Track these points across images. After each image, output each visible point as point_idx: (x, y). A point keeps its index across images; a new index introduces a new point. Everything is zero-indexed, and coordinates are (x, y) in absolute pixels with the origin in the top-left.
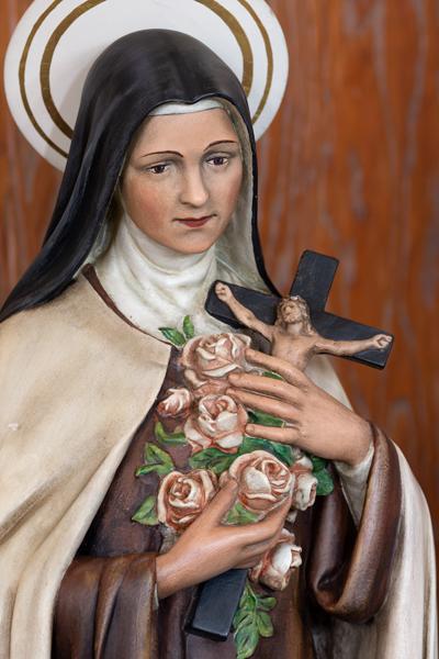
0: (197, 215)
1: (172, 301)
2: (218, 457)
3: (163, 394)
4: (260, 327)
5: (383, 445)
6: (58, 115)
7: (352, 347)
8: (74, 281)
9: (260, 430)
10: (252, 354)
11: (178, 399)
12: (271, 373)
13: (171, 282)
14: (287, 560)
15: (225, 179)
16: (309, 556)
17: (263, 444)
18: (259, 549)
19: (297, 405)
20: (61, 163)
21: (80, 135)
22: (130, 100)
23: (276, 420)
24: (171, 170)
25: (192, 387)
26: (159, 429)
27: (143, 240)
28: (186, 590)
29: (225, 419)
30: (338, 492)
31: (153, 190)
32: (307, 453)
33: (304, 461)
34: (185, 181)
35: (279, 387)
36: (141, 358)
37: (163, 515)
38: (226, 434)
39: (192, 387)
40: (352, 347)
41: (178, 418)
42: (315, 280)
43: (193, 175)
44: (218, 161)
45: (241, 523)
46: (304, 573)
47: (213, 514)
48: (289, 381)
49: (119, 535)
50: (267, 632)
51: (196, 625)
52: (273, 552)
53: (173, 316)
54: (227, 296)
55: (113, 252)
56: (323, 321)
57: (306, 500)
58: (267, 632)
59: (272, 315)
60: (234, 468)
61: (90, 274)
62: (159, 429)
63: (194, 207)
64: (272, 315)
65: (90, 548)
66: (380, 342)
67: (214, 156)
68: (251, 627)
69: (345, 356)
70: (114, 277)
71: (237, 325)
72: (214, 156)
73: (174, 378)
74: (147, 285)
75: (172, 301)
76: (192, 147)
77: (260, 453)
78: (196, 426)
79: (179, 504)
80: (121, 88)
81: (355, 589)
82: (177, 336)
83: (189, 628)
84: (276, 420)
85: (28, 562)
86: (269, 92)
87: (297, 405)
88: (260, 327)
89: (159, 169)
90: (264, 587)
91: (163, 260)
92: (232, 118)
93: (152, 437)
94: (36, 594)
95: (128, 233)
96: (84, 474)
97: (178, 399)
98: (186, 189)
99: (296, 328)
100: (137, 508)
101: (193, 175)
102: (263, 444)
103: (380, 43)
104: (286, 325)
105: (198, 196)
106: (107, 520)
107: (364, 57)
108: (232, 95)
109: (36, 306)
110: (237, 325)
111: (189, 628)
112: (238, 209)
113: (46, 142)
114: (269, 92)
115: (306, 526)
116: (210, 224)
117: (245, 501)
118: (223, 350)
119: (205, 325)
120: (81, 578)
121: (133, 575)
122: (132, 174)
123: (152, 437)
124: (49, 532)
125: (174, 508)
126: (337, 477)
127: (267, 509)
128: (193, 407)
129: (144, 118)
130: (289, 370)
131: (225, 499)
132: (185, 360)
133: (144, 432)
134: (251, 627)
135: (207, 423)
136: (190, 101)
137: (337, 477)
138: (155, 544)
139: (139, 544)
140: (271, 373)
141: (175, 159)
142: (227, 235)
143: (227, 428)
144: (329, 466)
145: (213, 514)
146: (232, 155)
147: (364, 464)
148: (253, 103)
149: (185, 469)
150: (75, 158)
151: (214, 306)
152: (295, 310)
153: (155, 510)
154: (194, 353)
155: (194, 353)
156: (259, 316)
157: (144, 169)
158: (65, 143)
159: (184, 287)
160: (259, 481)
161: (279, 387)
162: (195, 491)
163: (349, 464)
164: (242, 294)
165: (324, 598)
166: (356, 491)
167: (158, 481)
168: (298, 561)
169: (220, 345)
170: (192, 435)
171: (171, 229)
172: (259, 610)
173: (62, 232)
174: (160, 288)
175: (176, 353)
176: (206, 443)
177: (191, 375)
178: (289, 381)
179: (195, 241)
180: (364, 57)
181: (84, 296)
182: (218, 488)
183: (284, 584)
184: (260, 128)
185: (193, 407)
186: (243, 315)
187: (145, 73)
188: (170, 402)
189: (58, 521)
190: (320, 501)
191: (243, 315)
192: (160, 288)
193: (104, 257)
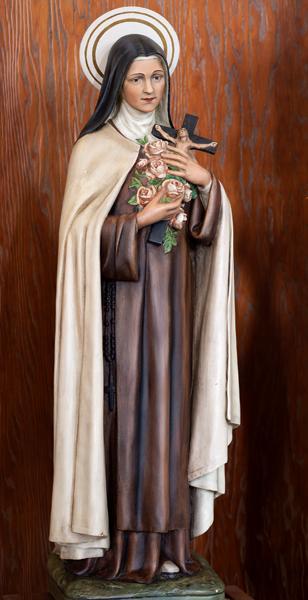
0: (149, 97)
1: (140, 130)
2: (158, 181)
3: (138, 161)
4: (172, 139)
5: (215, 180)
6: (113, 338)
7: (204, 146)
8: (105, 125)
9: (172, 172)
10: (169, 147)
11: (143, 162)
12: (175, 153)
13: (139, 123)
14: (182, 218)
15: (159, 85)
16: (189, 217)
17: (174, 177)
18: (172, 212)
19: (185, 164)
20: (99, 87)
21: (106, 76)
22: (126, 56)
23: (178, 169)
24: (140, 81)
25: (148, 159)
26: (136, 172)
27: (129, 108)
28: (146, 226)
29: (160, 168)
30: (199, 197)
31: (134, 88)
32: (189, 182)
33: (187, 184)
34: (145, 85)
35: (178, 157)
36: (129, 148)
37: (138, 201)
38: (160, 173)
39: (148, 159)
40: (204, 146)
41: (143, 169)
42: (190, 123)
43: (148, 81)
44: (157, 78)
45: (166, 202)
46: (188, 223)
47: (157, 199)
48: (181, 155)
49: (122, 208)
50: (175, 244)
51: (151, 240)
52: (178, 215)
53: (141, 136)
54: (159, 129)
55: (119, 115)
56: (192, 137)
57: (188, 198)
58: (175, 244)
59: (175, 134)
60: (163, 184)
61: (111, 122)
62: (136, 172)
63: (149, 94)
64: (175, 134)
65: (113, 212)
66: (213, 144)
67: (155, 76)
68: (169, 242)
69: (201, 150)
70: (119, 122)
71: (164, 139)
72: (155, 76)
73: (141, 155)
74: (131, 125)
75: (140, 130)
76: (148, 72)
77: (172, 180)
78: (149, 170)
79: (144, 197)
80: (122, 53)
81: (205, 230)
82: (142, 142)
83: (148, 241)
84: (178, 169)
85: (91, 217)
86: (174, 56)
87: (185, 164)
88: (172, 139)
89: (136, 80)
90: (174, 229)
91: (137, 116)
92: (162, 64)
93: (134, 175)
94: (95, 227)
95: (125, 107)
96: (110, 188)
97: (143, 162)
98: (145, 87)
99: (184, 139)
100: (129, 199)
101: (148, 81)
102: (174, 177)
103: (204, 73)
104: (180, 138)
105: (150, 90)
106: (119, 203)
107: (198, 78)
108: (162, 56)
109: (92, 132)
110: (164, 139)
111: (148, 241)
112: (163, 99)
113: (95, 81)
114: (174, 56)
115: (188, 207)
116: (154, 101)
117: (168, 196)
118: (159, 146)
119: (151, 138)
120: (110, 222)
121: (129, 220)
122: (126, 83)
123: (134, 175)
124: (98, 207)
125: (143, 199)
126: (199, 192)
127: (175, 198)
128: (149, 165)
129: (131, 62)
130: (182, 152)
131: (160, 194)
132: (145, 150)
133: (131, 173)
134: (169, 242)
135: (154, 170)
136: (147, 56)
137: (199, 192)
138: (136, 210)
139: (130, 210)
140: (175, 153)
141: (142, 77)
142: (158, 108)
143: (160, 171)
144: (196, 187)
145: (157, 199)
146: (162, 76)
147: (209, 186)
148: (169, 60)
149: (146, 186)
150: (104, 86)
151: (155, 132)
152: (184, 133)
153: (136, 200)
154: (149, 147)
155: (149, 147)
156: (171, 135)
157: (131, 80)
158: (101, 80)
159: (144, 125)
160: (172, 188)
161: (178, 157)
162: (150, 192)
163: (202, 186)
164: (164, 129)
165: (194, 234)
166: (205, 197)
167: (137, 190)
168: (186, 219)
169: (158, 144)
170: (148, 174)
171: (140, 104)
172: (238, 30)
173: (122, 553)
174: (136, 126)
175: (142, 148)
176: (153, 177)
177: (147, 154)
178: (181, 155)
179: (148, 107)
180: (198, 78)
181: (109, 129)
182: (157, 191)
183: (181, 227)
184: (172, 71)
185: (149, 165)
186: (165, 135)
187: (131, 47)
188: (140, 163)
189: (102, 203)
190: (193, 201)
191: (165, 135)
192: (136, 126)
193: (115, 116)
